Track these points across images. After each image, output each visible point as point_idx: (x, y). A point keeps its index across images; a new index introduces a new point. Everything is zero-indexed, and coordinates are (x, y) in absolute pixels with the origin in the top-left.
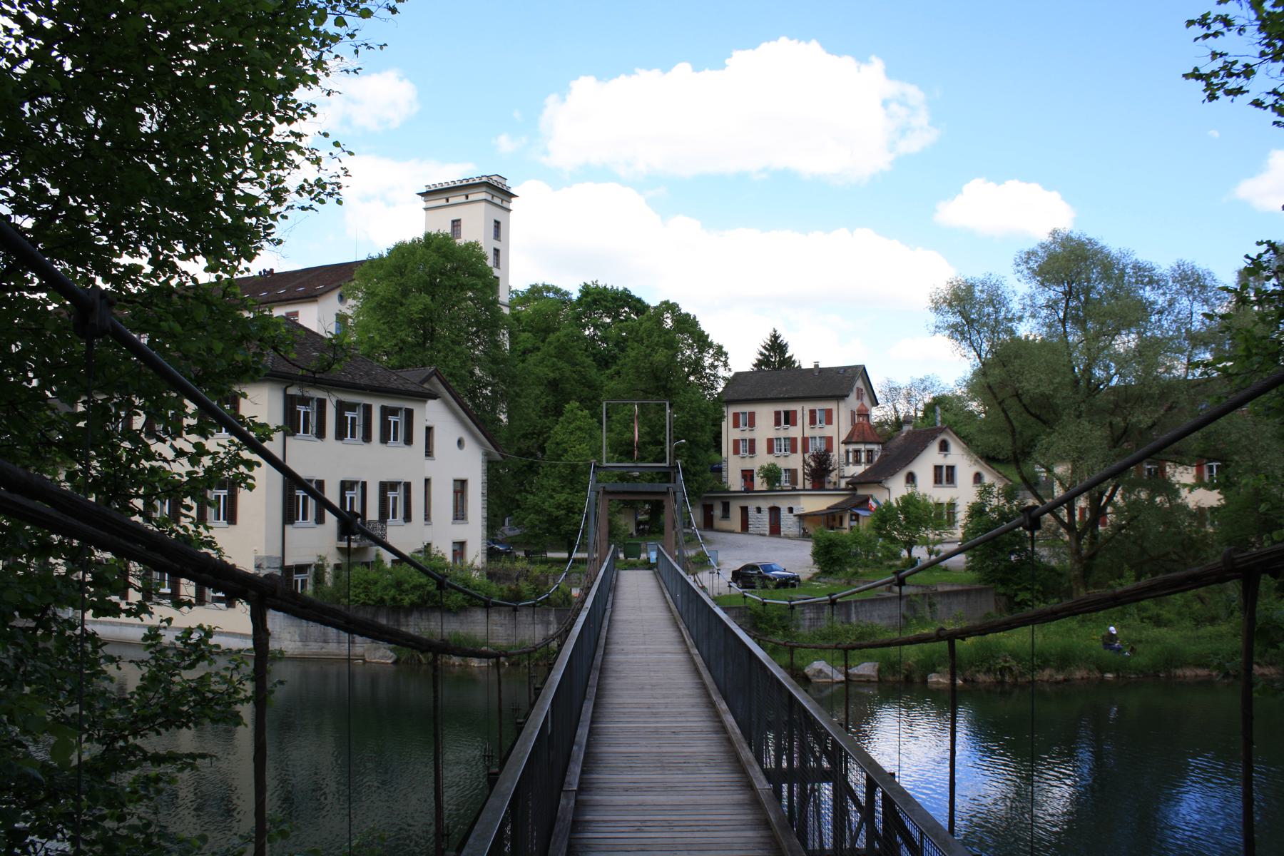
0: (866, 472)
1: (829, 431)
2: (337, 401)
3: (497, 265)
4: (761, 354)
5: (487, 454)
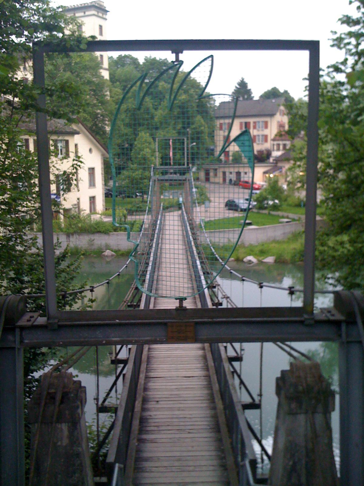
1: (266, 132)
4: (236, 87)
5: (103, 155)
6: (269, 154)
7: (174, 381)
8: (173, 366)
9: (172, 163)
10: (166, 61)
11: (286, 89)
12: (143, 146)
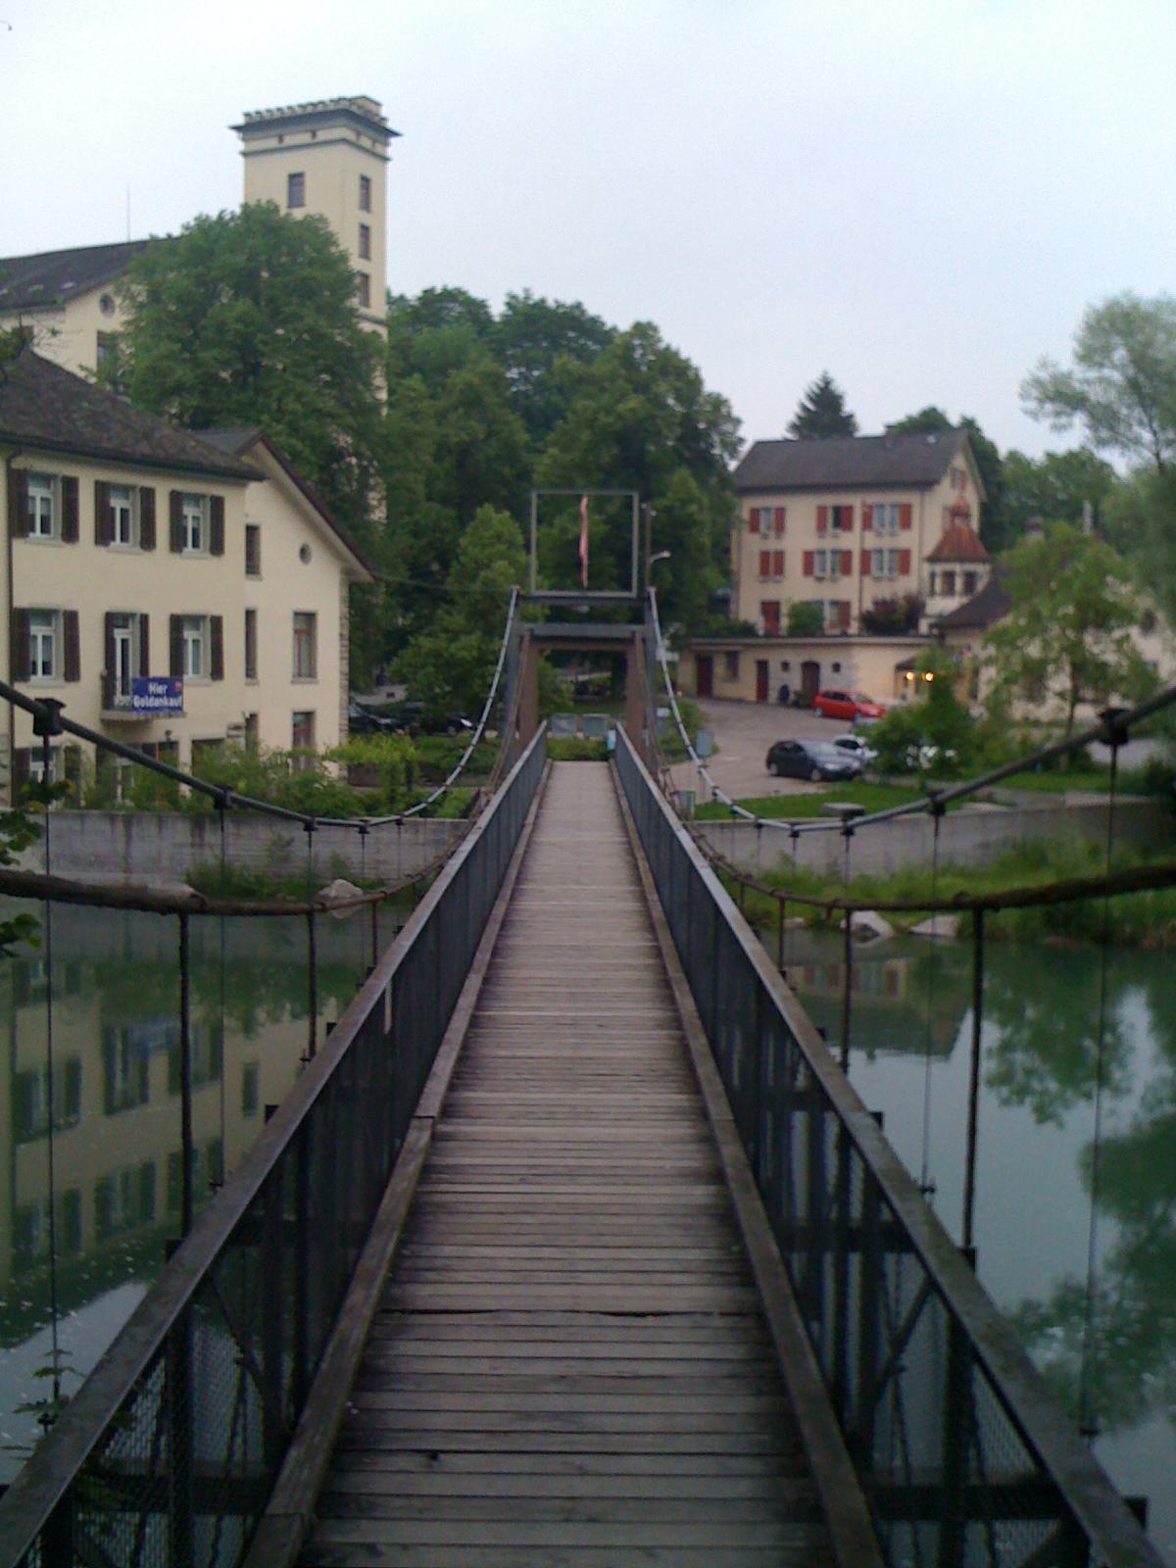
0: (963, 609)
1: (906, 539)
2: (97, 483)
3: (365, 254)
4: (805, 408)
5: (347, 572)
6: (914, 609)
7: (550, 1334)
8: (546, 1252)
9: (586, 583)
10: (577, 313)
11: (969, 415)
12: (487, 551)
